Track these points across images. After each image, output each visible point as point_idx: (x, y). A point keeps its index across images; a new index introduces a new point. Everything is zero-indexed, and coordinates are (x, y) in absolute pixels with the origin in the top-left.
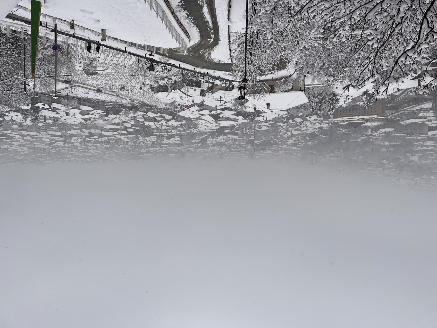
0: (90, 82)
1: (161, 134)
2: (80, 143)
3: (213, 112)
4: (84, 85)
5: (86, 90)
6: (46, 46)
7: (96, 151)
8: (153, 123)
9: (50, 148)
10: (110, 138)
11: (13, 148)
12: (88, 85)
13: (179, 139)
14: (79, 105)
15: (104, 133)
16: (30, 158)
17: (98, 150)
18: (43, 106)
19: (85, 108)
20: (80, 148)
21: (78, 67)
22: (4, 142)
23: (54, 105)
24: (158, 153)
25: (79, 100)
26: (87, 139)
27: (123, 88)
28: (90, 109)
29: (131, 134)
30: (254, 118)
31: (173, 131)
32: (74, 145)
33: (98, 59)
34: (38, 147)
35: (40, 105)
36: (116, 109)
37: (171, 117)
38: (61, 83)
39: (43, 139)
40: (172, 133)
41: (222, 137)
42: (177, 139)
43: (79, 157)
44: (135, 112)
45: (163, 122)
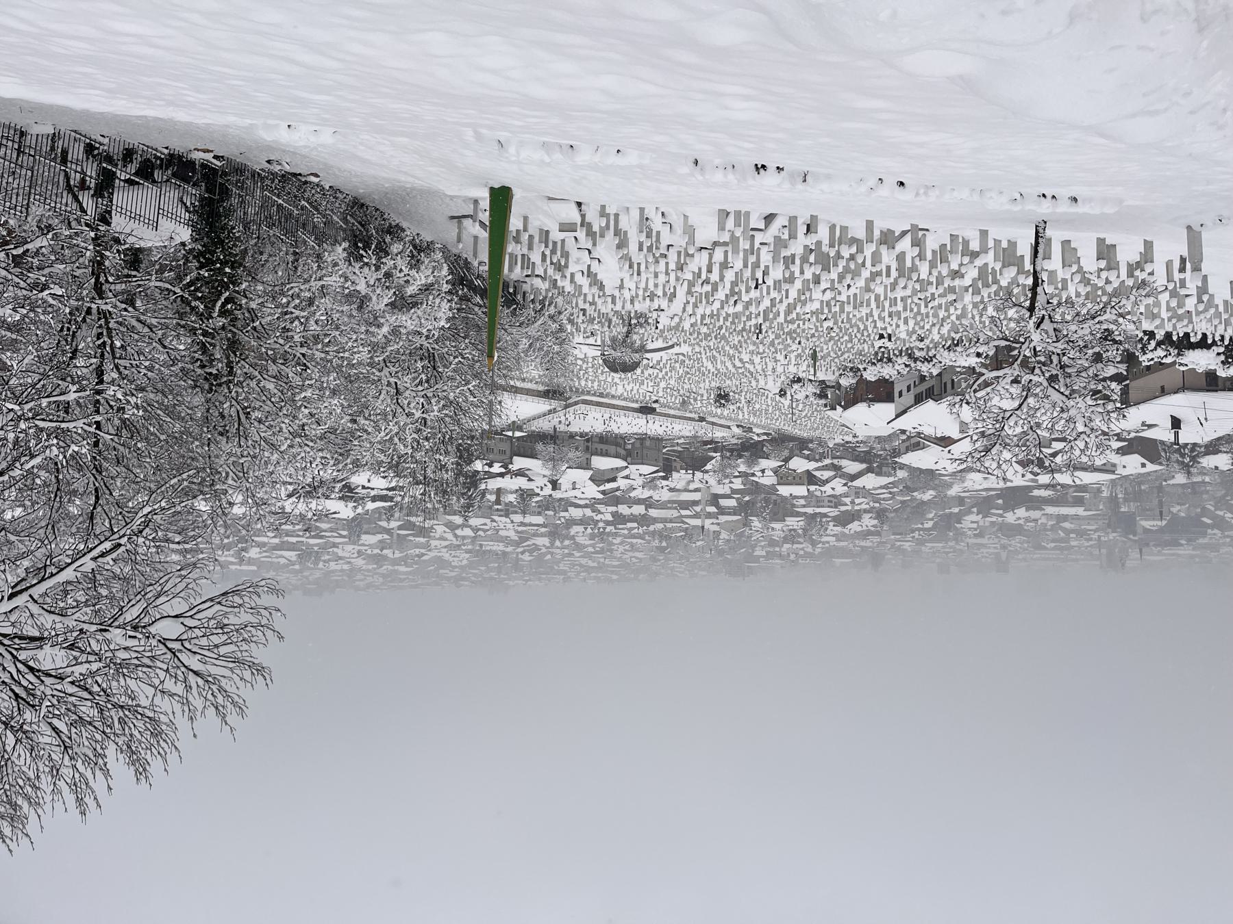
0: (620, 388)
2: (592, 537)
4: (602, 401)
5: (607, 413)
6: (411, 290)
7: (631, 554)
8: (804, 488)
9: (520, 550)
10: (669, 525)
11: (432, 554)
12: (613, 397)
13: (875, 522)
15: (653, 513)
16: (475, 575)
17: (638, 550)
18: (486, 468)
19: (602, 463)
20: (591, 549)
21: (585, 348)
23: (519, 463)
24: (801, 556)
25: (588, 440)
26: (609, 529)
28: (619, 463)
29: (729, 514)
30: (1193, 459)
32: (576, 543)
33: (655, 315)
34: (490, 551)
35: (478, 465)
36: (693, 457)
37: (864, 466)
39: (502, 533)
40: (857, 508)
41: (1021, 512)
42: (868, 522)
43: (588, 569)
44: (751, 462)
45: (838, 486)
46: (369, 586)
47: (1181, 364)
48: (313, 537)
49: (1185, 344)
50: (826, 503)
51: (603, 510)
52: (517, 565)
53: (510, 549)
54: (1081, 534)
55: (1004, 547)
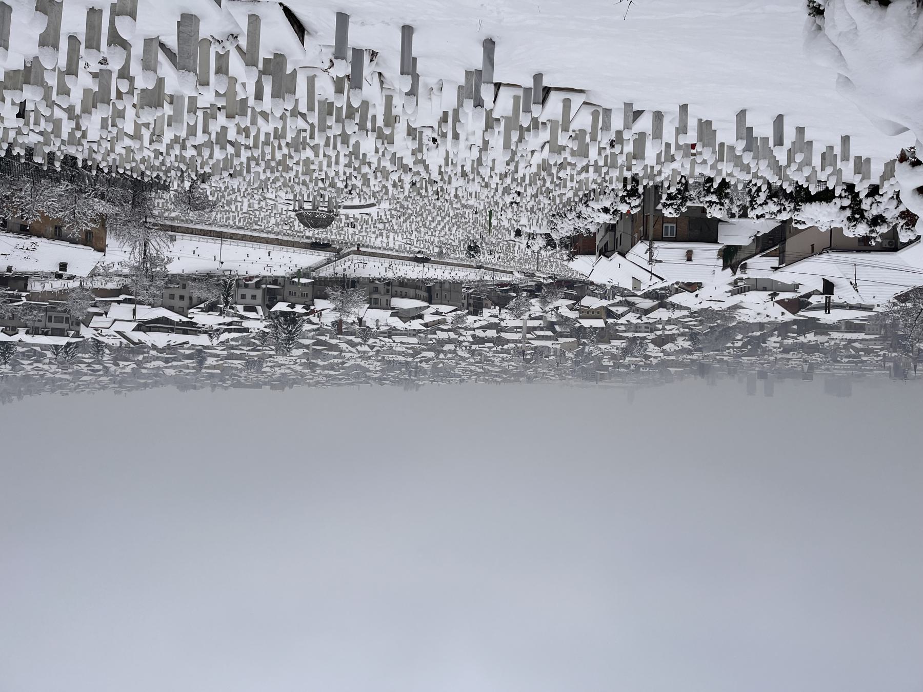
1: (637, 335)
3: (783, 296)
12: (375, 248)
13: (689, 343)
14: (388, 298)
15: (505, 335)
16: (393, 376)
22: (325, 355)
25: (388, 284)
27: (473, 249)
29: (567, 337)
31: (668, 327)
37: (656, 302)
38: (303, 251)
40: (666, 332)
46: (318, 383)
47: (798, 222)
48: (252, 350)
49: (801, 196)
50: (643, 329)
51: (464, 333)
52: (418, 370)
53: (410, 359)
54: (868, 352)
55: (806, 361)
